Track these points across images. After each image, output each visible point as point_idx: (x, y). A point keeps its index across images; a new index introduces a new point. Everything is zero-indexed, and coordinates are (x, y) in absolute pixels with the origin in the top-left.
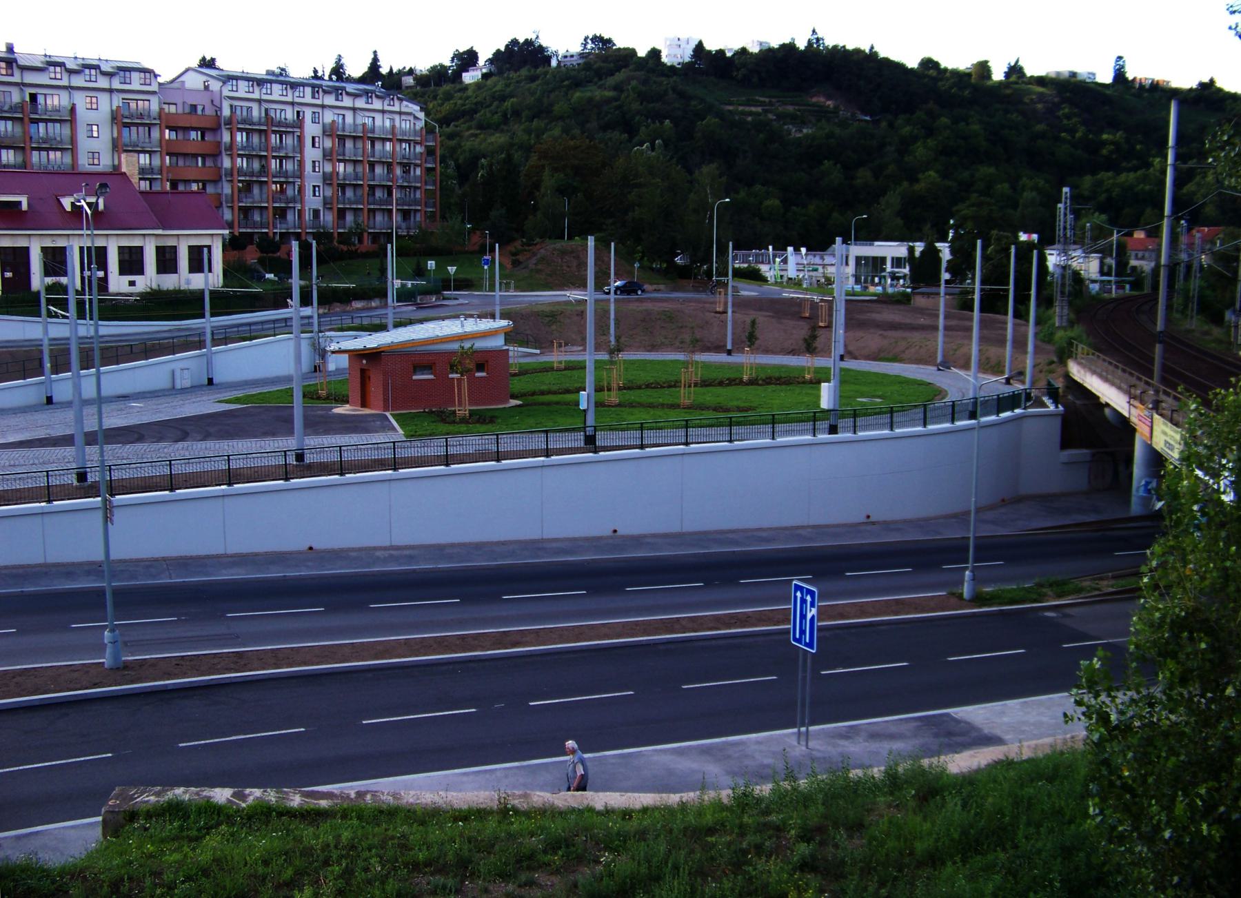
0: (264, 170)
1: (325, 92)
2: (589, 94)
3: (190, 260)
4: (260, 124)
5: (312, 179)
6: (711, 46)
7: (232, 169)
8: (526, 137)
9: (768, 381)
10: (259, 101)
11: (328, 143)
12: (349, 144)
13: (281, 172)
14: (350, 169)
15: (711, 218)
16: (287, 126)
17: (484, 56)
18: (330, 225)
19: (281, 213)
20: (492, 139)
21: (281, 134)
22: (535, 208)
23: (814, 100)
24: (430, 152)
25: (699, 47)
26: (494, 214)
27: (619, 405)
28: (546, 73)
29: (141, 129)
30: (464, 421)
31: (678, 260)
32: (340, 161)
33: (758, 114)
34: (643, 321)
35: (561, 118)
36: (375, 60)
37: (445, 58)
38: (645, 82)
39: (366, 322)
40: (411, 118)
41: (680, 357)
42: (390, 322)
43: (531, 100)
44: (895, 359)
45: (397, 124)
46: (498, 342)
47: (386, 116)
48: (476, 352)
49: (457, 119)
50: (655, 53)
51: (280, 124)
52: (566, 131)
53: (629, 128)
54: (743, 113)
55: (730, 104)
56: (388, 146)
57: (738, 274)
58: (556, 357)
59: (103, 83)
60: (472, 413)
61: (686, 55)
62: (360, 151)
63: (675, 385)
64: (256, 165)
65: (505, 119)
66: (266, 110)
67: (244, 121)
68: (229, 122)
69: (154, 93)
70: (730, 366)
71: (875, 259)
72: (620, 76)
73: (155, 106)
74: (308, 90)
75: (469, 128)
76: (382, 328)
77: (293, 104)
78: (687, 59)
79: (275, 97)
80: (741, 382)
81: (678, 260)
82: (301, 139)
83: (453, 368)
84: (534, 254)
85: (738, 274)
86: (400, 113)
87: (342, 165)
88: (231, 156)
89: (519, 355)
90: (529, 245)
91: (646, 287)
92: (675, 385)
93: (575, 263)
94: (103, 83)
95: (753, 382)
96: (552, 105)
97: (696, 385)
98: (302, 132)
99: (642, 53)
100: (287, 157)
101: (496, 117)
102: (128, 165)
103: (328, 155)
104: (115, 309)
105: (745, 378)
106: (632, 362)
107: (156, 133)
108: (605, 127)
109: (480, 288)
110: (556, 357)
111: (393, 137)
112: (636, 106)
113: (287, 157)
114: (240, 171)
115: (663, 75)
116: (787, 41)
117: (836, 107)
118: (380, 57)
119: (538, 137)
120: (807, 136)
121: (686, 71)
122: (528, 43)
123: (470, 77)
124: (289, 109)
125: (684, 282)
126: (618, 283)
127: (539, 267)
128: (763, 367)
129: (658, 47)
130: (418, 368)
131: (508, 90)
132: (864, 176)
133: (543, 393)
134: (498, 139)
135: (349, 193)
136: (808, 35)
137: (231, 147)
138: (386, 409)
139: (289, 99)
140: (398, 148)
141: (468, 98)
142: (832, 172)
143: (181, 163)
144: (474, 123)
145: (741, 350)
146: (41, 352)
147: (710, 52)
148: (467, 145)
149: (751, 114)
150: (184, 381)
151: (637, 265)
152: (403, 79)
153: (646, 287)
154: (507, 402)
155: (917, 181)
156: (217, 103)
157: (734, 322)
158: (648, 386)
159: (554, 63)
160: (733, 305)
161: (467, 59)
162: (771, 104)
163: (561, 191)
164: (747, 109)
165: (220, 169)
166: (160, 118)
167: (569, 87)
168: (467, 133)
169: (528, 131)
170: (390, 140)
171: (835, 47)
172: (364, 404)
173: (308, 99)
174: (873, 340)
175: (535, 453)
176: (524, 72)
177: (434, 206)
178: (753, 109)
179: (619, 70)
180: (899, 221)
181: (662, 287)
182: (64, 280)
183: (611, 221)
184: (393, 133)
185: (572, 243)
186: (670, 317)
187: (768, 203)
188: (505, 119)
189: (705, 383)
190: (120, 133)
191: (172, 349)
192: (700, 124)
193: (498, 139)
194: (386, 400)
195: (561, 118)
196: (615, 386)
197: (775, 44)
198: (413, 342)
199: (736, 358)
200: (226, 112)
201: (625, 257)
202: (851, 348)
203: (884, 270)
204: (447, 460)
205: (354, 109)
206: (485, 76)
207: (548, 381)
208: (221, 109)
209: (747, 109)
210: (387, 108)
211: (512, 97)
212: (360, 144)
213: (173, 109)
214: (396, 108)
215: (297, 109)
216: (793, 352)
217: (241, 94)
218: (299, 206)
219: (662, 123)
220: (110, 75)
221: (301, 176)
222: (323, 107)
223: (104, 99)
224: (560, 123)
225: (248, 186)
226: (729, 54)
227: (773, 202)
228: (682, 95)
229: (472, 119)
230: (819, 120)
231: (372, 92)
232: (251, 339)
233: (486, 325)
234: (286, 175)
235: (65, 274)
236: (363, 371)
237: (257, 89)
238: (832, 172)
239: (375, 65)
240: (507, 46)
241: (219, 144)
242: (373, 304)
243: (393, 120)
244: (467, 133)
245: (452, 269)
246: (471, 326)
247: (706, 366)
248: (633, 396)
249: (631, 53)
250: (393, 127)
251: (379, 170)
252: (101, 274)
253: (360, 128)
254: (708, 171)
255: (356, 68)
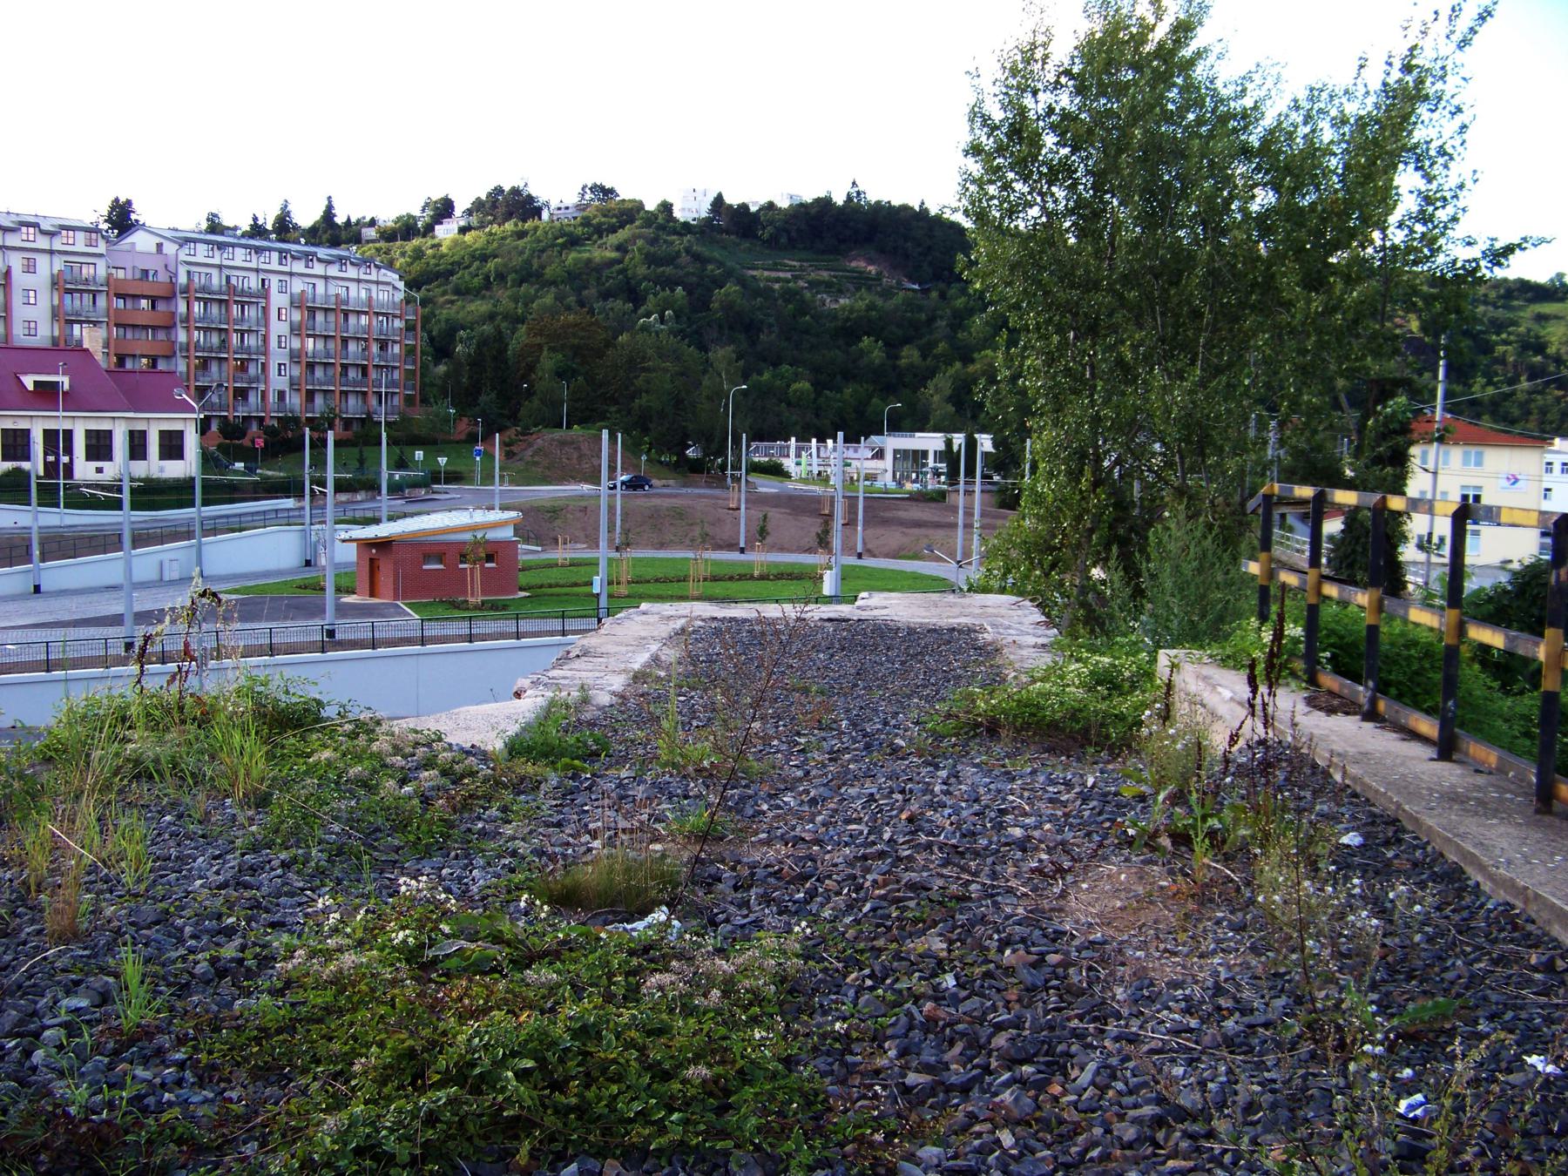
0: (224, 345)
1: (293, 258)
2: (586, 255)
3: (161, 446)
4: (220, 293)
5: (277, 356)
6: (732, 199)
7: (188, 344)
8: (512, 305)
9: (779, 577)
10: (220, 267)
11: (297, 316)
12: (320, 317)
13: (242, 348)
14: (320, 345)
15: (727, 405)
16: (251, 296)
17: (461, 206)
18: (297, 408)
19: (242, 394)
20: (472, 307)
21: (243, 304)
22: (530, 393)
23: (854, 264)
24: (410, 327)
25: (718, 201)
26: (483, 399)
27: (628, 596)
28: (536, 229)
29: (85, 295)
30: (477, 608)
31: (690, 452)
32: (309, 336)
33: (788, 281)
34: (651, 517)
35: (554, 283)
36: (330, 208)
37: (414, 206)
38: (653, 241)
39: (358, 514)
40: (390, 288)
41: (691, 555)
42: (384, 514)
43: (517, 261)
44: (916, 556)
45: (374, 295)
46: (507, 533)
47: (362, 285)
48: (488, 542)
49: (429, 282)
50: (666, 207)
51: (243, 293)
52: (560, 298)
53: (634, 296)
54: (768, 280)
55: (755, 268)
56: (364, 320)
57: (755, 468)
58: (560, 554)
59: (43, 243)
60: (483, 602)
61: (703, 209)
62: (332, 326)
63: (685, 579)
64: (215, 339)
65: (487, 284)
66: (228, 278)
67: (204, 289)
68: (186, 290)
69: (101, 255)
70: (742, 564)
71: (915, 452)
72: (623, 234)
73: (102, 271)
74: (275, 255)
75: (444, 293)
76: (377, 521)
77: (257, 271)
78: (704, 215)
79: (238, 262)
80: (752, 578)
81: (690, 452)
82: (265, 310)
83: (463, 558)
84: (530, 445)
85: (755, 468)
86: (377, 283)
87: (311, 340)
88: (188, 329)
89: (528, 552)
90: (523, 434)
91: (655, 482)
92: (685, 579)
93: (575, 455)
94: (43, 243)
95: (763, 577)
96: (543, 267)
97: (705, 579)
98: (268, 303)
99: (651, 206)
100: (249, 331)
101: (476, 280)
102: (91, 340)
103: (296, 330)
104: (80, 499)
105: (756, 573)
106: (641, 560)
107: (102, 301)
108: (606, 295)
109: (471, 481)
110: (560, 554)
111: (369, 310)
112: (642, 270)
113: (249, 331)
114: (197, 347)
115: (675, 232)
116: (822, 195)
117: (879, 274)
118: (335, 204)
119: (526, 305)
120: (843, 309)
121: (704, 230)
122: (516, 191)
123: (446, 232)
124: (253, 276)
125: (697, 477)
126: (624, 478)
127: (536, 459)
128: (777, 565)
129: (670, 200)
130: (427, 558)
131: (491, 248)
132: (910, 355)
133: (550, 586)
134: (479, 307)
135: (319, 372)
136: (848, 188)
137: (187, 319)
138: (396, 597)
139: (253, 265)
140: (374, 323)
141: (443, 256)
142: (871, 349)
143: (129, 335)
144: (449, 287)
145: (753, 548)
146: (30, 539)
147: (731, 206)
148: (444, 313)
149: (778, 280)
150: (172, 573)
151: (644, 458)
152: (364, 230)
153: (655, 482)
154: (514, 593)
155: (973, 361)
156: (172, 268)
157: (748, 519)
158: (657, 580)
159: (545, 215)
160: (747, 501)
161: (444, 209)
162: (802, 269)
163: (560, 374)
164: (774, 274)
165: (174, 343)
166: (108, 284)
167: (564, 246)
168: (442, 300)
169: (515, 299)
170: (365, 313)
171: (878, 203)
172: (372, 595)
173: (275, 266)
174: (894, 538)
175: (552, 633)
176: (509, 226)
177: (414, 388)
178: (782, 275)
179: (622, 226)
180: (951, 409)
181: (671, 482)
182: (26, 465)
183: (613, 409)
184: (370, 306)
185: (571, 433)
186: (679, 514)
187: (796, 386)
188: (487, 284)
189: (715, 579)
190: (61, 300)
191: (161, 540)
192: (719, 293)
193: (479, 307)
194: (396, 590)
195: (554, 283)
196: (623, 580)
197: (808, 197)
198: (424, 532)
199: (749, 557)
200: (182, 279)
201: (632, 448)
202: (869, 546)
203: (925, 465)
204: (470, 638)
205: (326, 278)
206: (463, 230)
207: (554, 575)
208: (176, 275)
209: (774, 274)
210: (363, 277)
211: (495, 256)
212: (332, 317)
213: (121, 274)
214: (373, 277)
215: (262, 276)
216: (810, 550)
217: (200, 259)
218: (262, 387)
219: (673, 291)
220: (51, 234)
221: (266, 353)
222: (291, 274)
223: (43, 262)
224: (553, 289)
225: (205, 364)
226: (753, 209)
227: (804, 385)
228: (697, 257)
229: (447, 282)
230: (858, 289)
231: (346, 258)
232: (241, 530)
233: (496, 516)
234: (248, 351)
235: (28, 459)
236: (372, 560)
237: (217, 253)
238: (871, 349)
239: (329, 214)
240: (489, 195)
241: (173, 314)
242: (359, 498)
243: (369, 290)
244: (442, 300)
245: (443, 461)
246: (480, 517)
247: (715, 563)
248: (640, 589)
249: (639, 206)
250: (370, 299)
251: (352, 347)
252: (65, 459)
253: (333, 299)
254: (721, 354)
255: (305, 217)
